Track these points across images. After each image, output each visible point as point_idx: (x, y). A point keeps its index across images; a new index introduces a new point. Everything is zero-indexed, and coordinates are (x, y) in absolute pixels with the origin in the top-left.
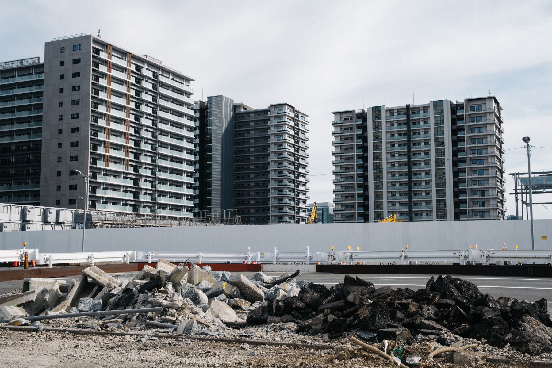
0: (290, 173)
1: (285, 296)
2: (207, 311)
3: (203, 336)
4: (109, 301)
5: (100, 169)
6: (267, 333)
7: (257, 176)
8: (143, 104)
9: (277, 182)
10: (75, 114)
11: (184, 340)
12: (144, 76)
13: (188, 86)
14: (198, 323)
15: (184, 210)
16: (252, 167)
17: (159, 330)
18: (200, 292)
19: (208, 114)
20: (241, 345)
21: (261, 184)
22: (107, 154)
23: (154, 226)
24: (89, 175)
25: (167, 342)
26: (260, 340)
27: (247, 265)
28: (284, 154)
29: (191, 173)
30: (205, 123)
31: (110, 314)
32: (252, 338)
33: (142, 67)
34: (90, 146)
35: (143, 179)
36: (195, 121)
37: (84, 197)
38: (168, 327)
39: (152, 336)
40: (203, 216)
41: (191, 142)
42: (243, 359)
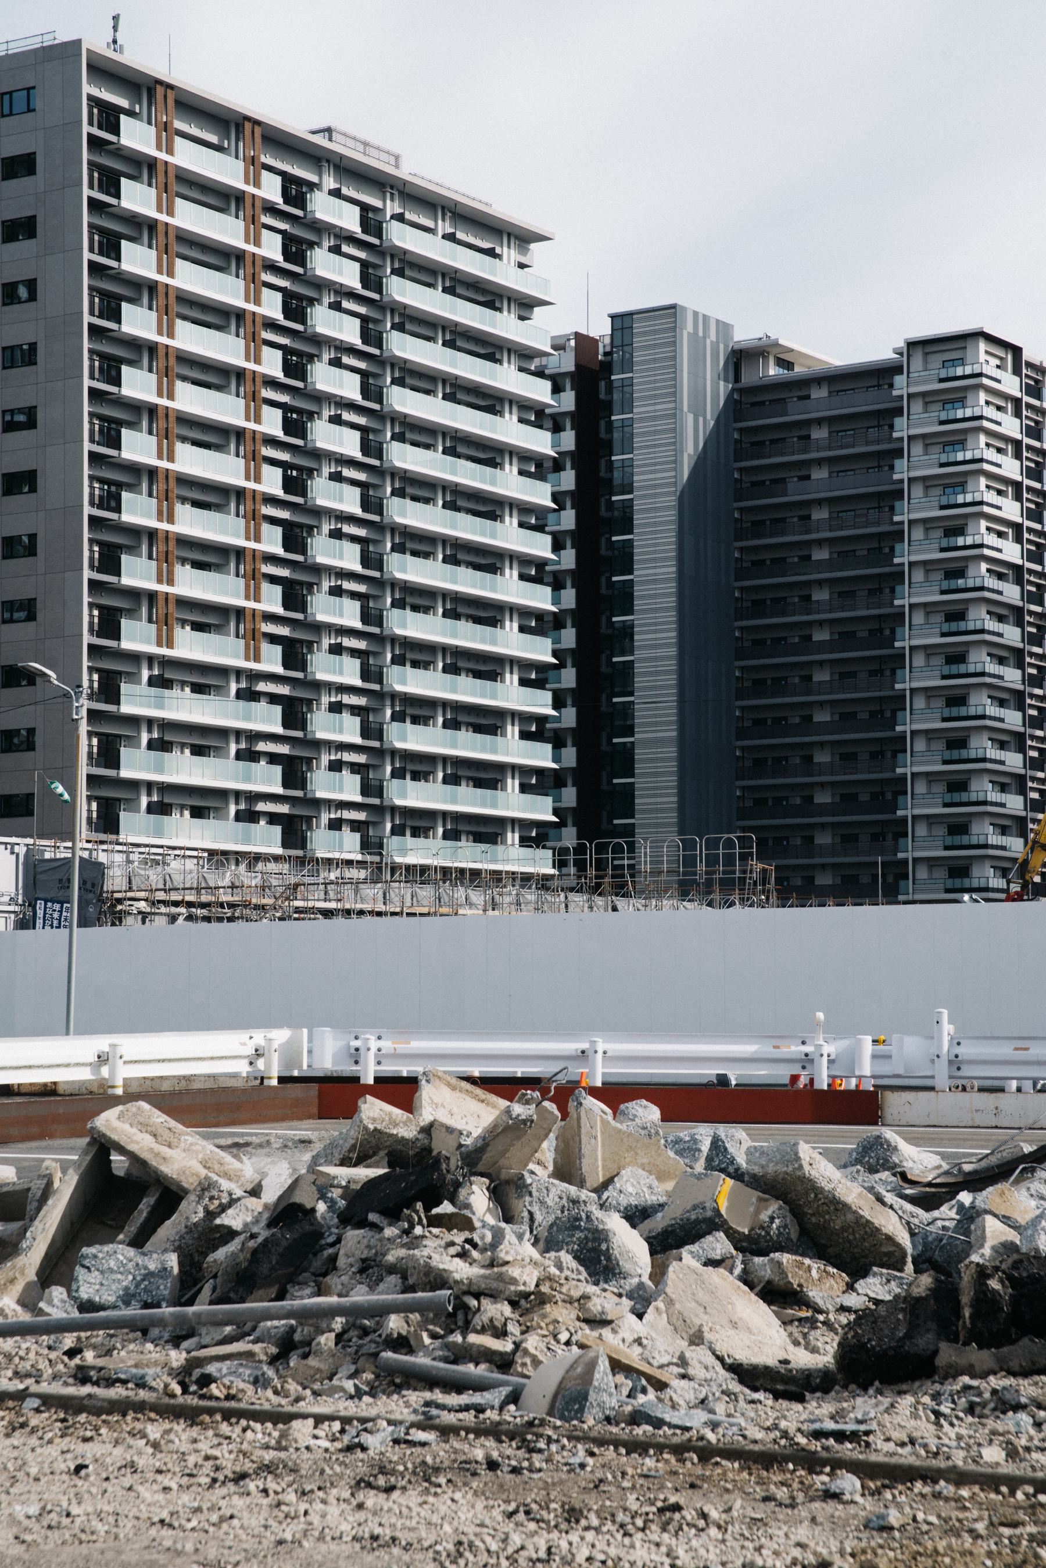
0: (1001, 661)
1: (1009, 1248)
2: (651, 1310)
3: (643, 1431)
4: (211, 1258)
5: (135, 658)
6: (937, 1424)
7: (842, 675)
8: (319, 357)
9: (940, 703)
10: (20, 411)
11: (554, 1447)
12: (320, 228)
13: (522, 266)
14: (613, 1369)
15: (513, 837)
16: (821, 636)
17: (438, 1396)
18: (616, 1225)
19: (616, 396)
20: (821, 1480)
21: (863, 716)
22: (164, 588)
23: (379, 914)
24: (85, 684)
25: (479, 1454)
26: (906, 1456)
27: (811, 1092)
28: (971, 572)
29: (542, 668)
30: (603, 435)
31: (219, 1322)
32: (868, 1445)
33: (312, 186)
34: (86, 554)
35: (325, 700)
36: (557, 429)
37: (72, 790)
38: (480, 1386)
39: (413, 1425)
40: (601, 865)
41: (539, 528)
42: (834, 1546)
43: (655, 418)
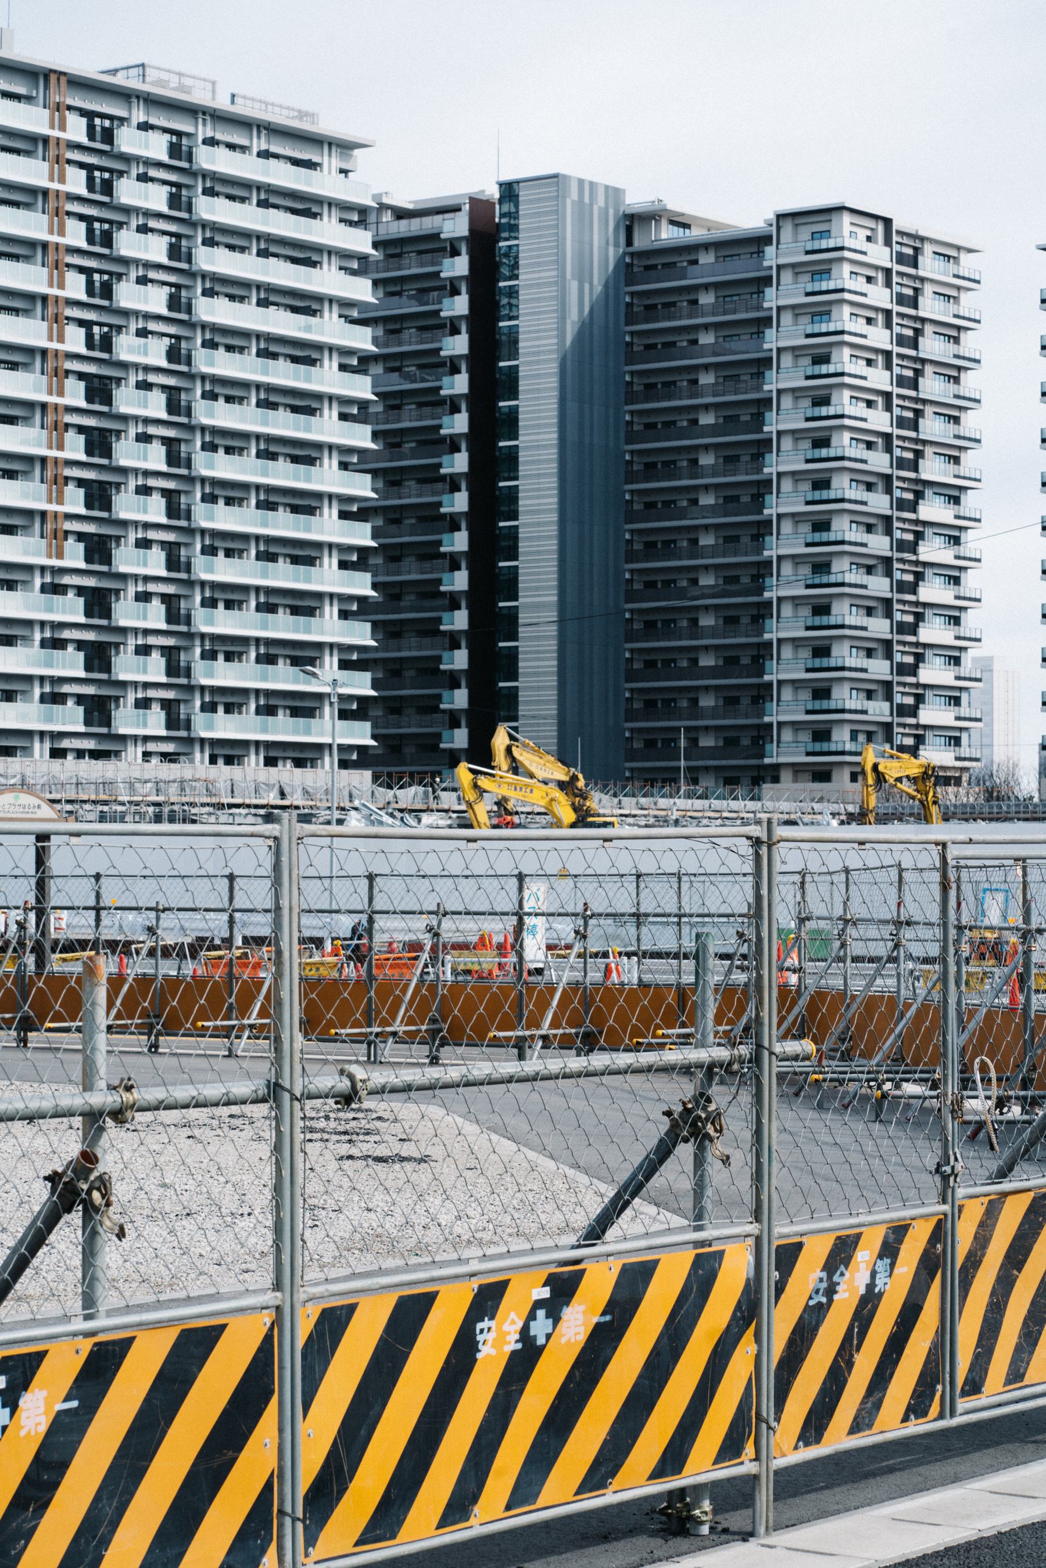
7: (728, 539)
43: (539, 285)
